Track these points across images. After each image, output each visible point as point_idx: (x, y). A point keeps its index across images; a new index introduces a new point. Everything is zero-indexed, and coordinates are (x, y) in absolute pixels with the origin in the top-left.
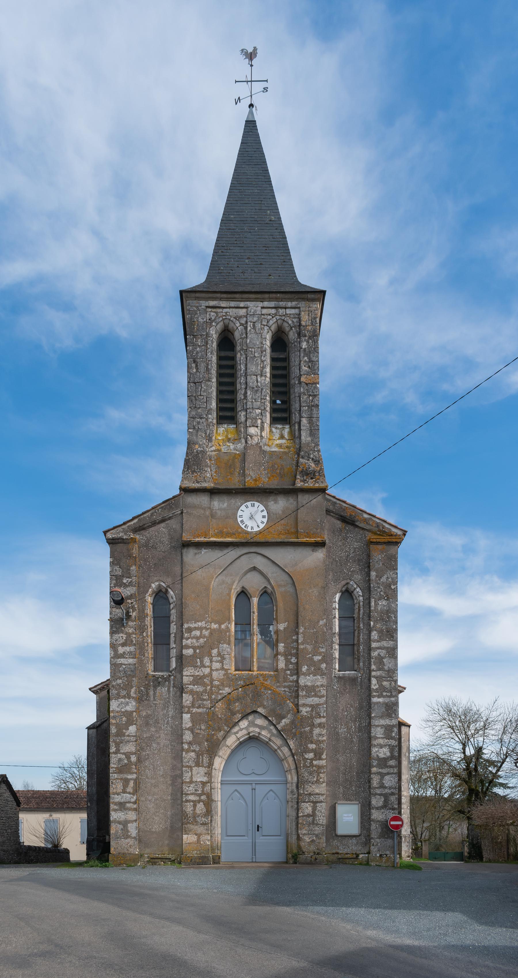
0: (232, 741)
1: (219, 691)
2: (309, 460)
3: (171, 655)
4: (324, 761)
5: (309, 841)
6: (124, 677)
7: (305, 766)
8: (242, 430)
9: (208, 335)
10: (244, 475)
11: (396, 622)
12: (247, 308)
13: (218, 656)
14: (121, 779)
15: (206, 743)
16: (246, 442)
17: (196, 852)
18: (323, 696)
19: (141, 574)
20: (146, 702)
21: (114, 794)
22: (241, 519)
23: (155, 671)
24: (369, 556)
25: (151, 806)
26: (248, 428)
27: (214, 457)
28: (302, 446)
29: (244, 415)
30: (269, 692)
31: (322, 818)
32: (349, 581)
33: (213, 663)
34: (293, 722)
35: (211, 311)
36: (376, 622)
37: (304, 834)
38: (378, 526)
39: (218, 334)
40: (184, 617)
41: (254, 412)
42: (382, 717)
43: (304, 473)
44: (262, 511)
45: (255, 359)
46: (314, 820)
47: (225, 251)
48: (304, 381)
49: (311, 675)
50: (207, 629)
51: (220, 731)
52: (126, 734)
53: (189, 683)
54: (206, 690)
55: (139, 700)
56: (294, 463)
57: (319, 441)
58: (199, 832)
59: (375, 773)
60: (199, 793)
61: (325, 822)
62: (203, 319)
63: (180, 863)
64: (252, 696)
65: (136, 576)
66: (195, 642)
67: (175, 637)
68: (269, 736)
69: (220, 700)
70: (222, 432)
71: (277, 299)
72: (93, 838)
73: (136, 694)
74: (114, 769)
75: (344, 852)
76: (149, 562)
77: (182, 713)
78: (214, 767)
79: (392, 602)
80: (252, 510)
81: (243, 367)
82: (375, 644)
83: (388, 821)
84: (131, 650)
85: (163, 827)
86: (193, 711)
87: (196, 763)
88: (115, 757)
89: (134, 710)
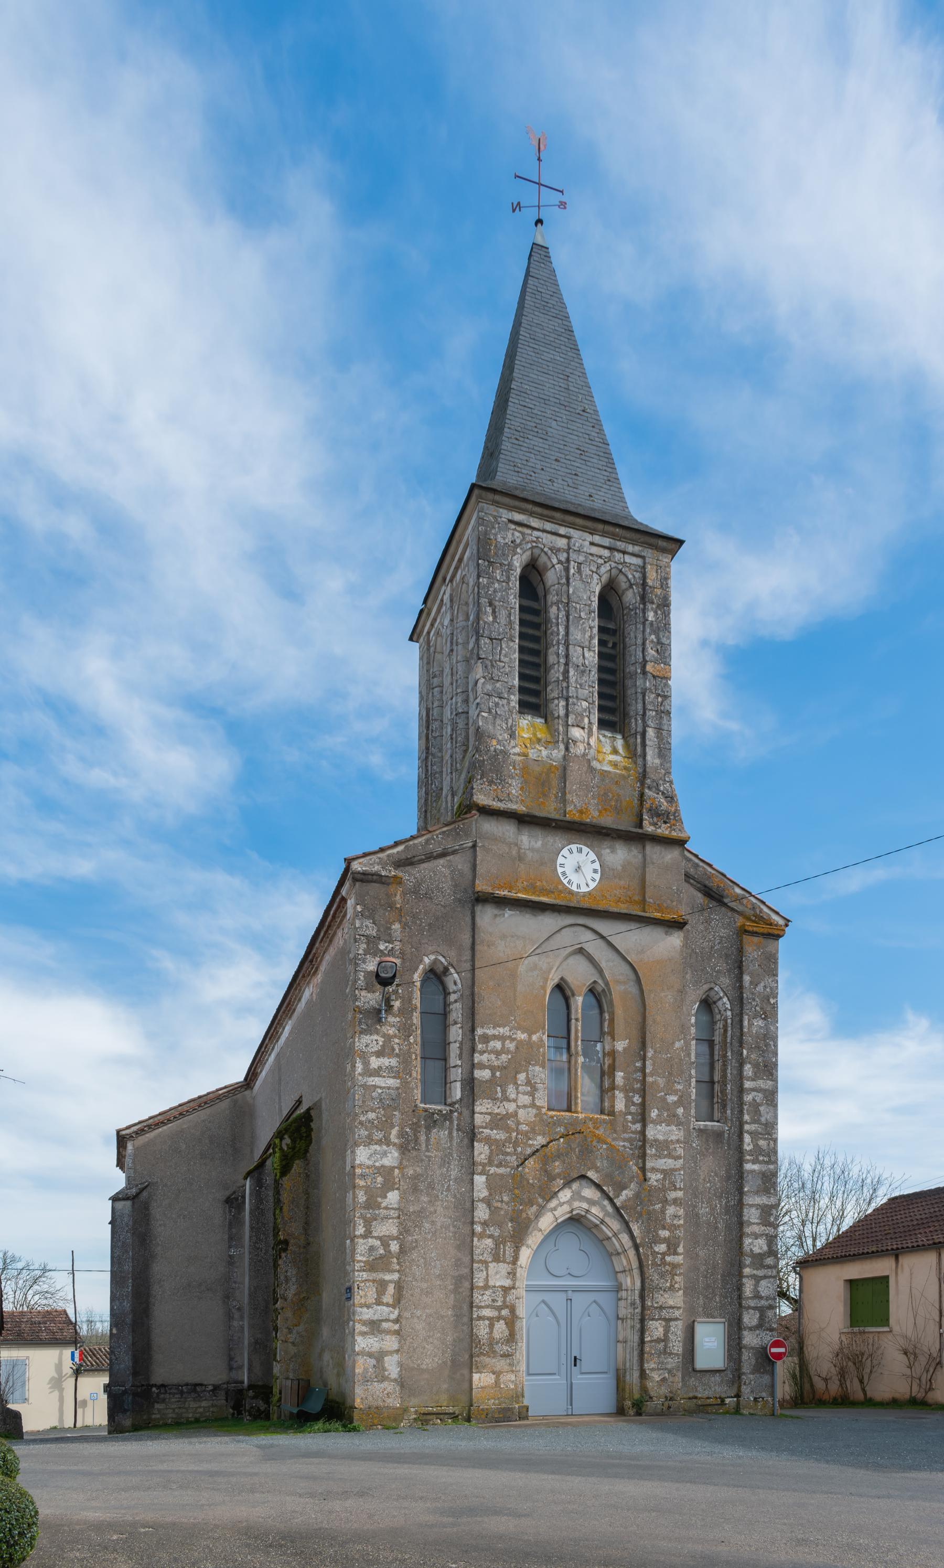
0: (546, 1222)
1: (527, 1141)
2: (658, 794)
3: (452, 1078)
4: (681, 1257)
5: (658, 1379)
6: (379, 1108)
7: (654, 1264)
8: (561, 728)
9: (510, 565)
10: (564, 801)
11: (776, 1054)
12: (569, 538)
13: (526, 1084)
14: (374, 1281)
15: (510, 1225)
16: (567, 749)
17: (493, 1401)
18: (679, 1157)
19: (407, 939)
20: (414, 1153)
21: (361, 1307)
22: (562, 870)
23: (424, 1101)
24: (741, 951)
25: (420, 1326)
28: (648, 770)
29: (563, 706)
30: (604, 1146)
31: (677, 1346)
32: (712, 985)
33: (520, 1095)
34: (637, 1195)
35: (515, 529)
36: (750, 1050)
37: (653, 1370)
40: (477, 1017)
42: (757, 1193)
43: (653, 812)
44: (593, 862)
45: (581, 622)
46: (666, 1347)
47: (521, 439)
48: (651, 671)
49: (663, 1125)
50: (513, 1040)
51: (532, 1206)
52: (383, 1205)
53: (484, 1124)
54: (510, 1138)
55: (404, 1149)
56: (636, 794)
57: (671, 768)
58: (497, 1369)
59: (747, 1277)
60: (498, 1304)
61: (681, 1349)
62: (504, 539)
63: (468, 1420)
64: (580, 1151)
65: (400, 941)
66: (494, 1059)
67: (461, 1048)
68: (601, 1215)
69: (530, 1156)
70: (525, 727)
71: (614, 536)
72: (124, 1388)
73: (398, 1138)
74: (362, 1264)
75: (705, 1396)
76: (420, 920)
77: (473, 1174)
78: (519, 1263)
79: (772, 1022)
80: (581, 858)
81: (562, 630)
82: (748, 1083)
83: (766, 1348)
84: (391, 1064)
85: (440, 1362)
86: (491, 1172)
87: (493, 1255)
88: (364, 1244)
89: (396, 1165)
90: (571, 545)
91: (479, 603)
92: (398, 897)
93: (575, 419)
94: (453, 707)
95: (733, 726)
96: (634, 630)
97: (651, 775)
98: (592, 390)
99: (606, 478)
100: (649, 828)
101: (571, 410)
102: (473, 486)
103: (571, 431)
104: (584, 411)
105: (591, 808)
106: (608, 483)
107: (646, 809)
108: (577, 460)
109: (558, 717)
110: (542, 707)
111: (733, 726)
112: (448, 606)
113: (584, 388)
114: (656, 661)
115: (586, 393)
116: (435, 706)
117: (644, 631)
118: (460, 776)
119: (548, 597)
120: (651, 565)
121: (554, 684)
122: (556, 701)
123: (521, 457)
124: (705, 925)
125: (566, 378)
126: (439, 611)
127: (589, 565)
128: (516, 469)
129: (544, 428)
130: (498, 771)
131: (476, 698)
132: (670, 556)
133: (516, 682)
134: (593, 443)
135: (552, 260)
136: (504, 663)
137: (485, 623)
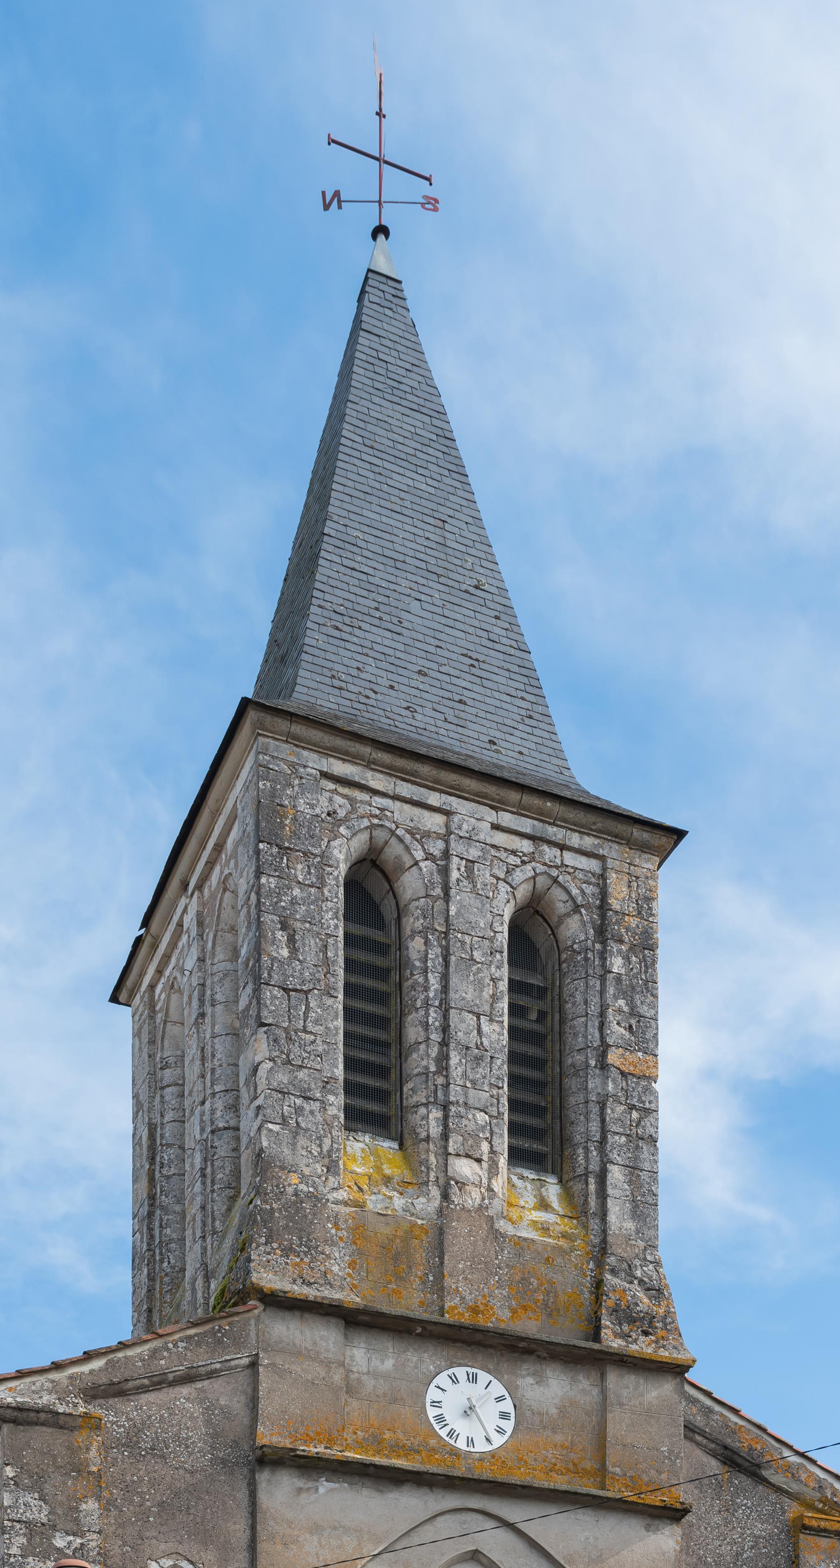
2: (631, 1282)
8: (433, 1159)
9: (325, 859)
10: (439, 1288)
12: (448, 813)
16: (445, 1196)
22: (437, 1411)
26: (450, 1157)
27: (346, 1221)
28: (609, 1239)
29: (437, 1119)
38: (820, 1487)
39: (349, 865)
41: (470, 1116)
44: (500, 1399)
45: (474, 968)
48: (617, 1064)
56: (587, 1281)
57: (656, 1238)
62: (312, 806)
65: (100, 1532)
70: (359, 1154)
71: (541, 816)
76: (141, 1494)
81: (434, 981)
90: (453, 827)
91: (259, 923)
92: (93, 1453)
93: (458, 601)
94: (206, 1118)
95: (762, 1214)
96: (582, 989)
97: (618, 1250)
98: (495, 550)
99: (523, 712)
100: (611, 1341)
101: (451, 583)
102: (245, 704)
103: (450, 622)
104: (477, 587)
105: (496, 1303)
106: (528, 721)
107: (607, 1308)
108: (463, 675)
109: (428, 1139)
110: (393, 1121)
111: (762, 1214)
112: (194, 933)
113: (477, 545)
114: (627, 1047)
115: (482, 555)
116: (166, 1119)
117: (602, 992)
118: (221, 1243)
119: (404, 920)
120: (617, 872)
121: (418, 1080)
122: (423, 1111)
123: (346, 661)
124: (726, 1514)
125: (440, 524)
126: (173, 944)
127: (491, 865)
128: (337, 683)
129: (395, 612)
130: (301, 1230)
131: (256, 1098)
132: (657, 860)
133: (339, 1071)
134: (497, 646)
135: (409, 304)
136: (315, 1035)
137: (273, 959)
